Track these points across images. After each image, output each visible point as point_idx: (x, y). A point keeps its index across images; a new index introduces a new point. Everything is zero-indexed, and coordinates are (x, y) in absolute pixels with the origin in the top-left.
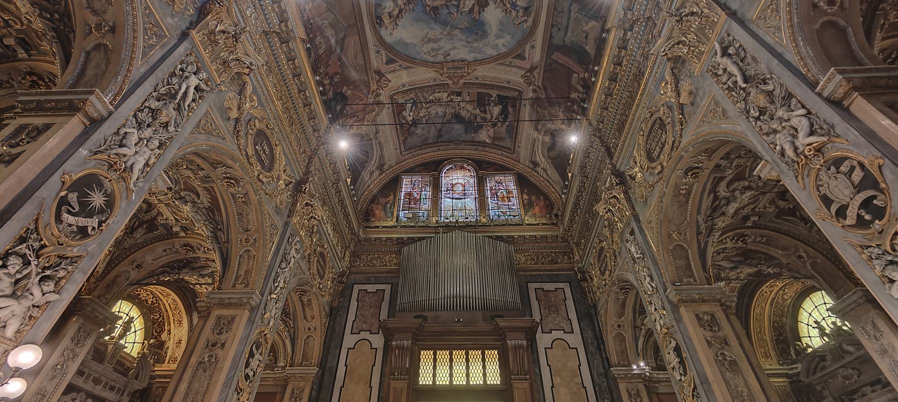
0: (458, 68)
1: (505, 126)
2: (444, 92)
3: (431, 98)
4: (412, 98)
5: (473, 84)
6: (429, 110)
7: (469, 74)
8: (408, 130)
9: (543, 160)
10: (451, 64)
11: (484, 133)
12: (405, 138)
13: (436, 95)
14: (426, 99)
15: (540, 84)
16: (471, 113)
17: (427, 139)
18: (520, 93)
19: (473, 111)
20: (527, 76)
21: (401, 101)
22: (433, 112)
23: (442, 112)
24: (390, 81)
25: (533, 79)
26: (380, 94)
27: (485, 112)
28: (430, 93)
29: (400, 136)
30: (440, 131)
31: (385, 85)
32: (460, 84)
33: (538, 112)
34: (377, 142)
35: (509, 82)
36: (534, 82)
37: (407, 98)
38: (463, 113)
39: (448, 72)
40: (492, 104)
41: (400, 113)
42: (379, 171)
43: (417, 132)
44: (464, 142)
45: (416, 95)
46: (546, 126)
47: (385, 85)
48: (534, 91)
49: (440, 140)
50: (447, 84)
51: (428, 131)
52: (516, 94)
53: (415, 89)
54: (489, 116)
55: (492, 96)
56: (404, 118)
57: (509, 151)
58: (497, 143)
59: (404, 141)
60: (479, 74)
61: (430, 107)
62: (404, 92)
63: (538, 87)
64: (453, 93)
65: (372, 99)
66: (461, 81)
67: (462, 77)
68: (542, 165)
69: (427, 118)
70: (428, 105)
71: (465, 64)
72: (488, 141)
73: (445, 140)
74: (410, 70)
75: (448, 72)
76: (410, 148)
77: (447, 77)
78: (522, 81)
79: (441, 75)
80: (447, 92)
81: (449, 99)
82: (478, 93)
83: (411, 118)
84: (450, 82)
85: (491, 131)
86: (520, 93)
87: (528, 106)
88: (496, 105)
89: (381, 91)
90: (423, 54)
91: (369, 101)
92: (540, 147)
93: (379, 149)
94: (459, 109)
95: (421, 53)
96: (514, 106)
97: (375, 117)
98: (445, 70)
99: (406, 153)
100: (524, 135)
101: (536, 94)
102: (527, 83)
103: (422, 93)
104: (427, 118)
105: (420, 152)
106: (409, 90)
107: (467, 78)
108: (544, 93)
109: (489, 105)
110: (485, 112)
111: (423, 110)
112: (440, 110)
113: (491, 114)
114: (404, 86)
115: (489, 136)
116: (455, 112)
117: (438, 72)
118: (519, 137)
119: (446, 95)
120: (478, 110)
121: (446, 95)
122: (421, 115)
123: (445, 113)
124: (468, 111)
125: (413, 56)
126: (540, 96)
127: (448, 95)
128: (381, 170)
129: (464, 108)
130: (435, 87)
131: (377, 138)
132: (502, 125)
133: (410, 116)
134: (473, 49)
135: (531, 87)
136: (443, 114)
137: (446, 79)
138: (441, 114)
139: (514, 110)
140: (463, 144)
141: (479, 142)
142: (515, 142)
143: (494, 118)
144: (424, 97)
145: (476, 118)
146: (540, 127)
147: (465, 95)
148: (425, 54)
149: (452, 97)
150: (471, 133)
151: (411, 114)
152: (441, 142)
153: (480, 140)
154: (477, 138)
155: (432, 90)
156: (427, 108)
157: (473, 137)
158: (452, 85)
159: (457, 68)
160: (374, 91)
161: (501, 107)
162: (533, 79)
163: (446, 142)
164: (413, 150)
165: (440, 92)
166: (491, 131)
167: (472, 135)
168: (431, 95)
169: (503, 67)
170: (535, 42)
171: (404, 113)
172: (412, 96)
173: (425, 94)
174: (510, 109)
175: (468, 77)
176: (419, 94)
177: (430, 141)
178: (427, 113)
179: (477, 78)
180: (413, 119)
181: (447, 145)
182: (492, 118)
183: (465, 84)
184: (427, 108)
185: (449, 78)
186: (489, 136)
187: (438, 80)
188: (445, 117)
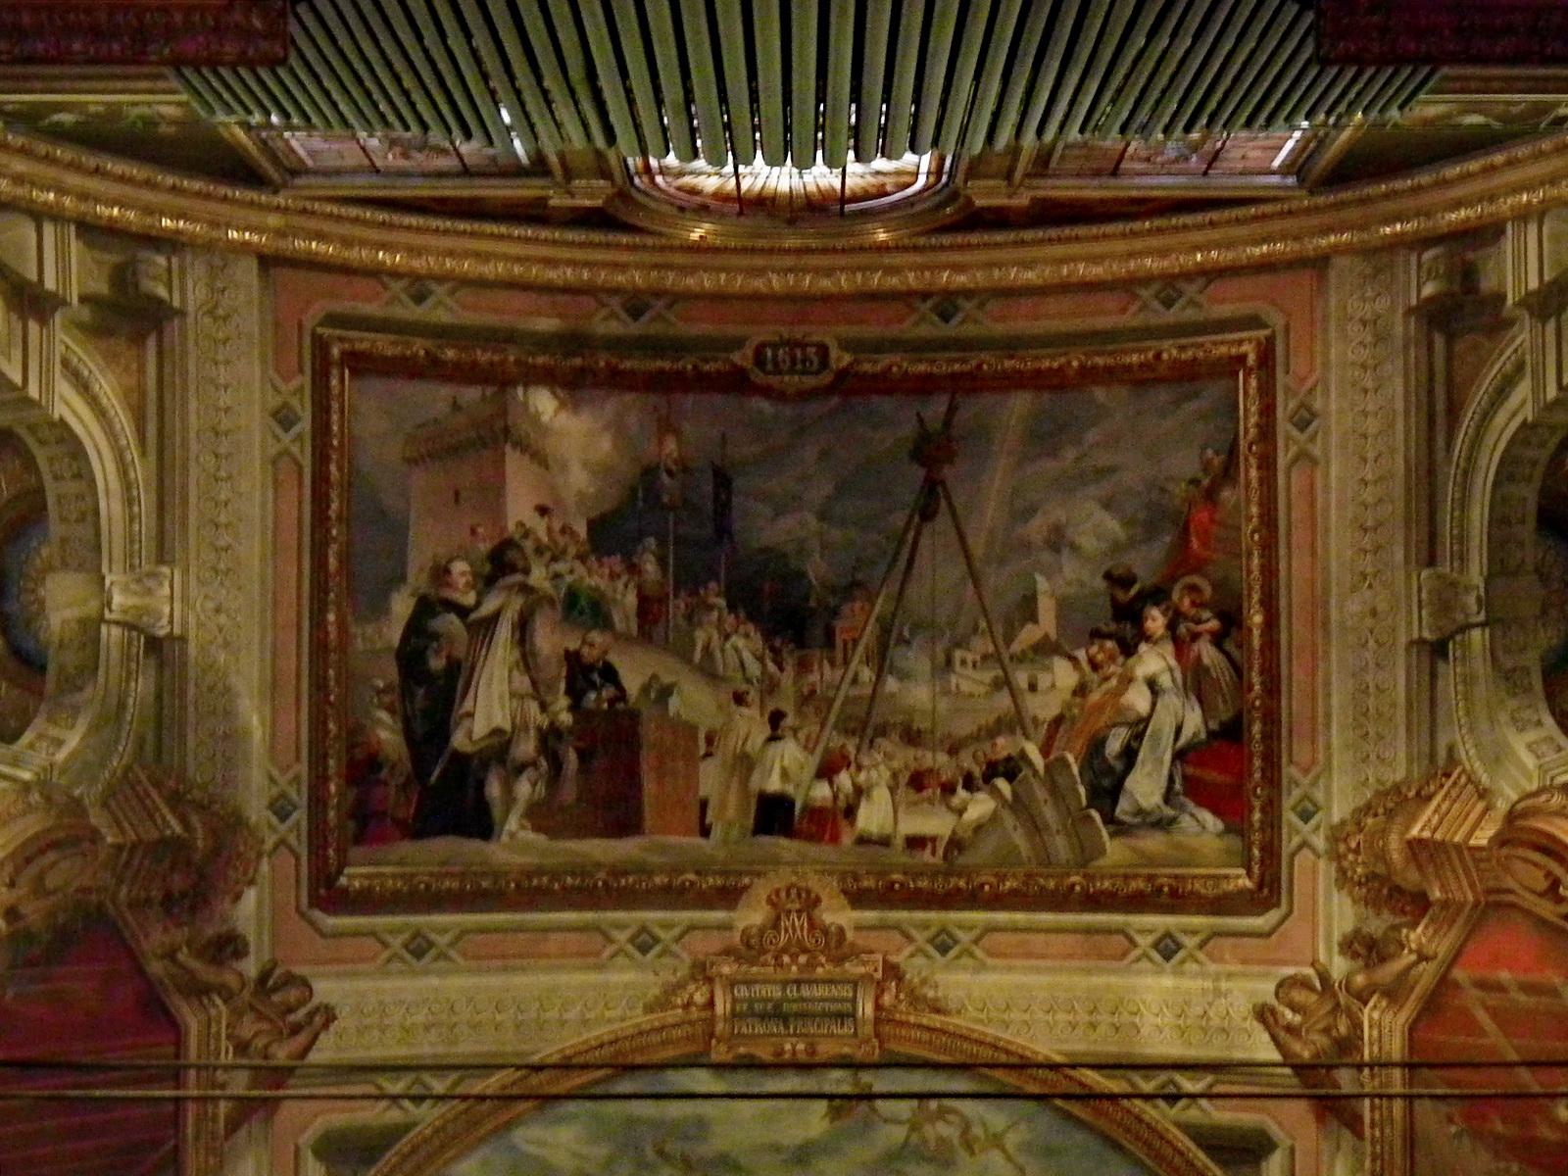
0: (778, 1014)
1: (417, 578)
2: (885, 842)
3: (980, 806)
4: (1119, 829)
5: (675, 896)
6: (1004, 701)
7: (702, 972)
8: (1182, 562)
9: (68, 406)
10: (826, 1049)
11: (578, 480)
12: (1211, 495)
13: (936, 823)
14: (1019, 805)
15: (192, 1021)
16: (686, 657)
17: (1044, 438)
18: (328, 894)
19: (669, 671)
20: (296, 1030)
21: (1202, 827)
22: (971, 680)
23: (904, 676)
24: (1264, 1015)
25: (247, 1028)
26: (1348, 946)
27: (582, 674)
28: (984, 852)
29: (1250, 532)
30: (930, 502)
31: (1299, 996)
32: (761, 890)
33: (175, 800)
34: (1444, 568)
35: (419, 947)
36: (237, 1014)
37: (1153, 843)
38: (744, 647)
39: (846, 992)
40: (526, 747)
41: (1229, 734)
42: (1487, 284)
43: (1112, 525)
44: (736, 383)
45: (1085, 853)
46: (94, 729)
47: (1299, 996)
48: (229, 947)
49: (936, 408)
50: (858, 899)
51: (1029, 512)
52: (354, 877)
53: (1094, 901)
54: (550, 640)
55: (540, 816)
56: (1196, 682)
57: (364, 341)
58: (471, 394)
59: (1228, 472)
60: (629, 976)
61: (992, 732)
62: (1177, 900)
63: (199, 991)
64: (824, 823)
65: (1416, 936)
66: (752, 915)
67: (750, 949)
68: (63, 339)
69: (1029, 635)
70: (1004, 747)
71: (733, 1039)
72: (543, 402)
73: (885, 404)
74: (1109, 1046)
75: (846, 992)
76: (1187, 375)
77: (855, 953)
78: (326, 989)
79: (893, 971)
80: (863, 840)
81: (844, 779)
82: (626, 824)
83: (1154, 661)
84: (837, 915)
85: (519, 509)
86: (328, 894)
87: (256, 811)
88: (499, 747)
89: (1340, 967)
90: (1012, 1140)
91: (1443, 947)
92: (111, 507)
93: (1450, 491)
94: (771, 687)
95: (1026, 1147)
96: (364, 768)
97: (1424, 799)
98: (866, 1008)
99: (1221, 347)
100: (252, 550)
101: (210, 931)
102: (289, 980)
103: (1046, 859)
104: (1029, 635)
105: (1107, 316)
106: (1138, 903)
107: (715, 942)
108: (156, 968)
109: (550, 739)
110: (582, 674)
111: (1044, 707)
112: (916, 693)
113: (527, 658)
114: (1167, 947)
115: (539, 458)
116: (803, 667)
117: (916, 1000)
118: (297, 505)
119: (873, 817)
120: (632, 683)
121: (873, 817)
122: (1063, 675)
123: (881, 660)
124: (709, 673)
125: (1080, 1137)
126: (180, 935)
127: (850, 812)
128: (1468, 276)
129: (739, 699)
130: (940, 886)
131: (1445, 601)
132: (441, 573)
133: (1152, 684)
134: (673, 1147)
135: (251, 967)
136: (898, 655)
137: (872, 940)
138: (916, 659)
139: (355, 734)
140: (742, 358)
141: (617, 380)
142: (321, 457)
143: (504, 632)
144: (1035, 827)
145: (649, 610)
146: (142, 687)
147: (731, 812)
148: (996, 1141)
149: (822, 792)
150: (684, 468)
151: (1138, 699)
152: (925, 386)
153: (612, 404)
154: (632, 420)
155: (966, 872)
156: (1015, 723)
157: (667, 426)
158: (828, 891)
159: (785, 1019)
160: (1393, 993)
161: (459, 741)
162: (247, 1028)
163: (884, 384)
164: (1170, 350)
165: (916, 842)
166: (519, 509)
167: (671, 445)
168: (979, 828)
169: (467, 1048)
170: (273, 451)
171: (1194, 722)
172: (1115, 851)
173: (1020, 839)
174: (387, 734)
175: (705, 945)
176: (1061, 847)
177: (1019, 404)
178: (1021, 678)
179: (644, 941)
180: (1128, 650)
181: (878, 347)
182: (523, 628)
183: (729, 897)
184: (1015, 723)
185: (837, 947)
186: (539, 458)
187: (920, 937)
188: (885, 630)
